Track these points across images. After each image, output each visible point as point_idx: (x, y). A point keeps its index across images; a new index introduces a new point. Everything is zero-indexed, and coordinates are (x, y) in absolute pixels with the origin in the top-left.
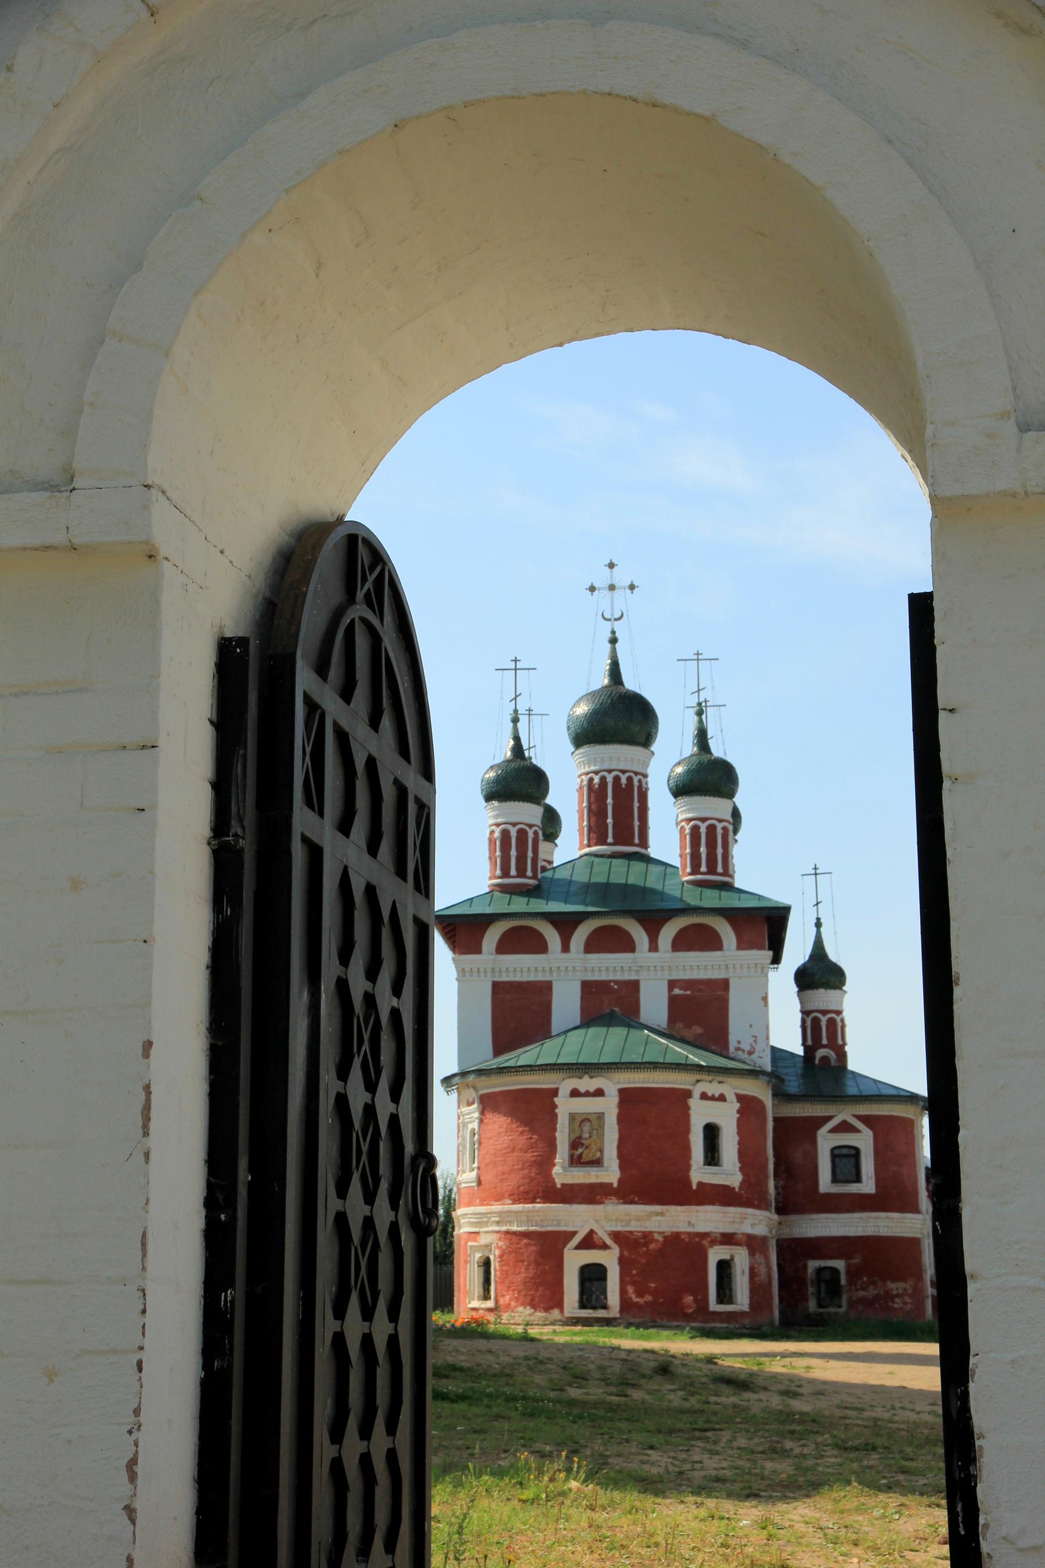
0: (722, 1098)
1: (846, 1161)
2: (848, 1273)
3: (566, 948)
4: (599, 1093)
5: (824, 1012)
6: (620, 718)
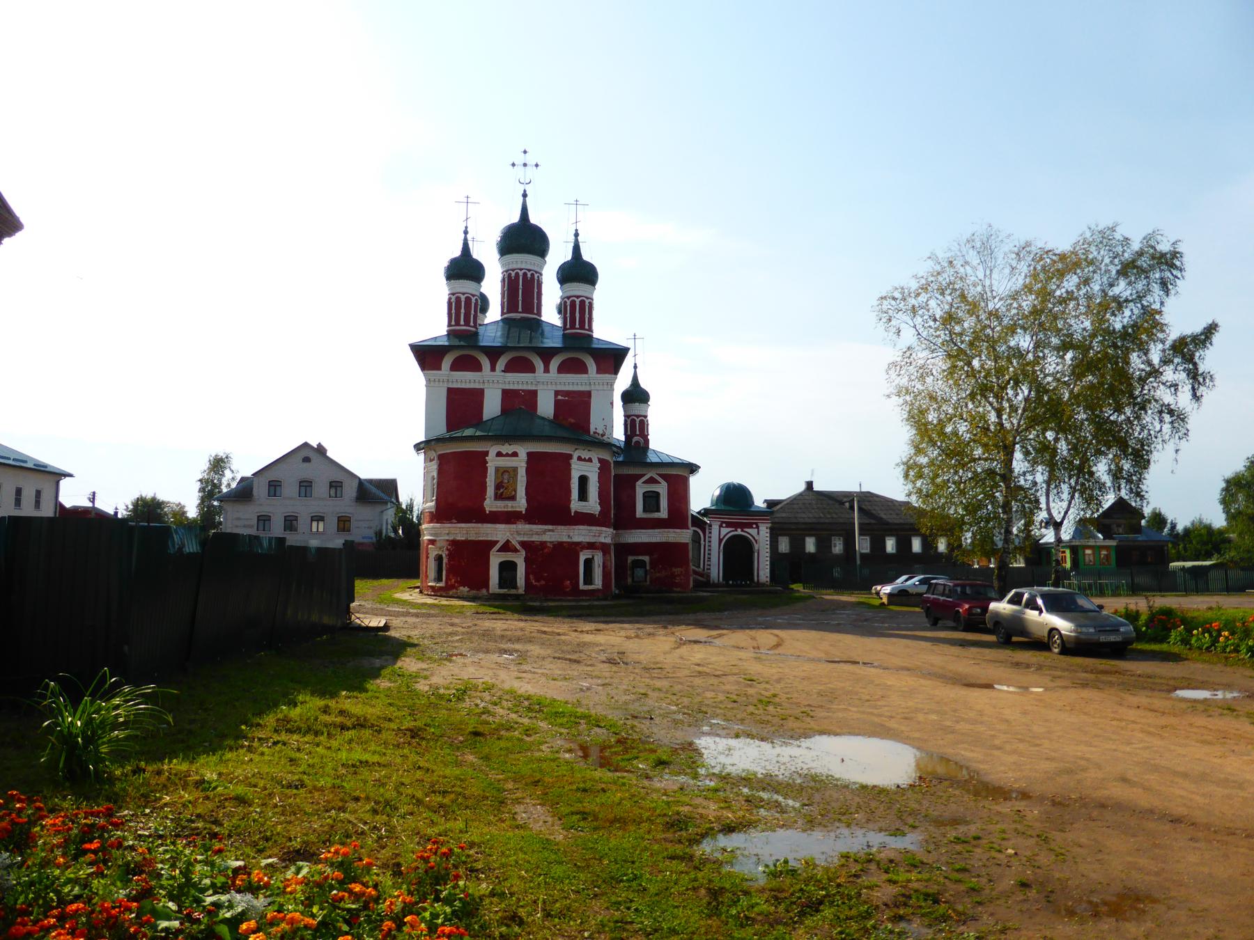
0: (590, 460)
1: (652, 500)
2: (651, 563)
3: (493, 369)
4: (515, 454)
5: (638, 416)
6: (524, 239)
